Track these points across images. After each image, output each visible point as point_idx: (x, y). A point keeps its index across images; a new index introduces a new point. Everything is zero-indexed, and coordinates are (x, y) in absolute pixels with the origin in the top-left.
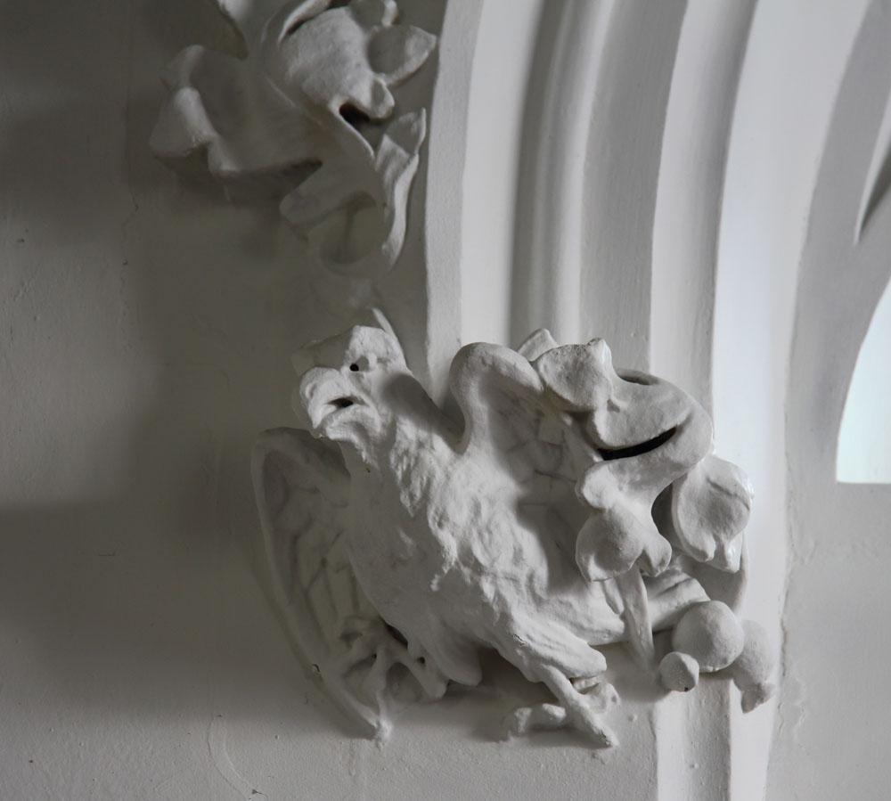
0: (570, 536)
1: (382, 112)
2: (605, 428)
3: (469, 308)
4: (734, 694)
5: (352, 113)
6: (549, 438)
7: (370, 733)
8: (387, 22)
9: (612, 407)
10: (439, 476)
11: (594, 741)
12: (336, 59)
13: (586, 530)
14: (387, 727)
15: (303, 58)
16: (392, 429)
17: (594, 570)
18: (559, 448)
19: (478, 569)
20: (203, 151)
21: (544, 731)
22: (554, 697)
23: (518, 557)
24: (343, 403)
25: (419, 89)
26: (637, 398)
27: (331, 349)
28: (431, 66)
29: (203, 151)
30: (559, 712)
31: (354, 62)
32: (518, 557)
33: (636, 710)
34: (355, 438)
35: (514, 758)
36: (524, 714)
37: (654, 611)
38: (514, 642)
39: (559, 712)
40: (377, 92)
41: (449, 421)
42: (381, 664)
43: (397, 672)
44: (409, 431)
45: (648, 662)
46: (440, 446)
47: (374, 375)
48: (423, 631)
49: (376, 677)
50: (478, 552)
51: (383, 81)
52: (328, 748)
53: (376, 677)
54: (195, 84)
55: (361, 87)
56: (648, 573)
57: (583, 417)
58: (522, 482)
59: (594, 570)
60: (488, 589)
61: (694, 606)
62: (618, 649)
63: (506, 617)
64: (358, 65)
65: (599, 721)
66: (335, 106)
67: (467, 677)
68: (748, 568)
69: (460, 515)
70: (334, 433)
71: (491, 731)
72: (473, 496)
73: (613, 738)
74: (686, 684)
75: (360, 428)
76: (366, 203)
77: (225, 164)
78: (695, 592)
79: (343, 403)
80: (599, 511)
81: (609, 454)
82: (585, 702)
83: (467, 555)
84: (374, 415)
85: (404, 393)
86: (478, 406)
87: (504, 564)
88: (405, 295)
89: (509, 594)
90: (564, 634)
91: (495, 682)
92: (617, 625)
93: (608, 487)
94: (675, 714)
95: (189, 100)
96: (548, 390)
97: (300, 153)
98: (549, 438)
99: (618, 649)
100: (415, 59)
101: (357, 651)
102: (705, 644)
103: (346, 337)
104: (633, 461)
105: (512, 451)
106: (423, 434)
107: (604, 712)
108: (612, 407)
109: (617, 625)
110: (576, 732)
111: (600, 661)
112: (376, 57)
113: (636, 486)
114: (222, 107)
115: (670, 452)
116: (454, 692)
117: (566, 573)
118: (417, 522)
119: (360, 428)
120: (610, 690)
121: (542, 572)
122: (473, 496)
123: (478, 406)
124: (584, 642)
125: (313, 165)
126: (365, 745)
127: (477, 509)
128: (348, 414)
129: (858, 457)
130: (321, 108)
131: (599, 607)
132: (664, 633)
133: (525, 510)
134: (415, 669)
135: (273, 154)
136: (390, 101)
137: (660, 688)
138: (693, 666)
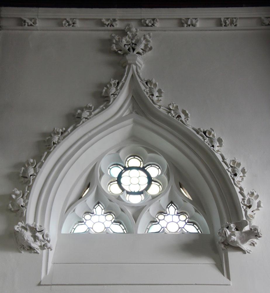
0: (35, 238)
1: (24, 206)
2: (38, 230)
3: (30, 221)
4: (50, 250)
5: (22, 206)
6: (33, 230)
7: (22, 253)
8: (25, 199)
9: (38, 228)
10: (25, 233)
11: (38, 253)
12: (21, 202)
13: (37, 237)
14: (23, 252)
15: (18, 202)
16: (22, 230)
17: (37, 241)
18: (35, 231)
19: (28, 240)
20: (11, 209)
21: (34, 252)
22: (35, 250)
23: (31, 240)
24: (18, 228)
25: (27, 204)
26: (41, 227)
27: (17, 224)
28: (28, 203)
29: (11, 209)
30: (35, 251)
31: (246, 189)
32: (31, 240)
33: (42, 251)
34: (19, 231)
35: (32, 255)
36: (33, 251)
37: (43, 243)
38: (31, 246)
39: (35, 251)
40: (24, 204)
41: (26, 229)
42: (22, 248)
43: (24, 248)
44: (23, 230)
45: (42, 247)
46: (25, 231)
47: (20, 226)
48: (25, 246)
49: (22, 248)
50: (28, 239)
51: (24, 204)
52: (19, 254)
53: (22, 248)
54: (11, 204)
55: (22, 204)
56: (41, 241)
57: (36, 229)
58: (32, 234)
59: (37, 241)
60: (29, 242)
61: (46, 243)
62: (40, 246)
63: (31, 244)
64: (245, 188)
65: (39, 252)
66: (20, 205)
67: (29, 249)
68: (51, 240)
69: (26, 236)
70: (17, 230)
71: (31, 253)
72: (28, 235)
73: (40, 253)
74: (45, 249)
75: (19, 230)
76: (22, 213)
77: (13, 210)
78: (47, 242)
79: (18, 228)
80: (37, 236)
81: (38, 232)
82: (37, 250)
83: (27, 239)
84: (20, 229)
85: (23, 227)
86: (28, 228)
87: (30, 240)
88: (24, 219)
89: (31, 242)
90: (36, 245)
91: (31, 249)
92: (40, 245)
93: (38, 234)
94: (45, 251)
95: (10, 205)
96: (33, 227)
97: (18, 209)
98: (33, 230)
99: (40, 246)
100: (27, 202)
101: (21, 247)
102: (47, 246)
103: (18, 223)
104: (40, 232)
105: (31, 231)
106: (24, 230)
107: (39, 251)
108: (38, 228)
109: (40, 245)
110: (37, 253)
111: (39, 247)
112: (24, 202)
113: (40, 234)
114: (13, 205)
115: (43, 232)
116: (28, 250)
117: (35, 241)
118: (23, 237)
119: (19, 230)
120: (40, 249)
121: (33, 241)
122: (28, 235)
123: (28, 228)
124: (37, 246)
125: (19, 210)
126: (21, 254)
127: (28, 236)
128: (18, 229)
129: (64, 231)
130: (19, 206)
131: (39, 243)
132: (44, 245)
133: (32, 236)
134: (25, 248)
135: (16, 209)
136: (25, 205)
137: (44, 249)
138: (46, 248)
